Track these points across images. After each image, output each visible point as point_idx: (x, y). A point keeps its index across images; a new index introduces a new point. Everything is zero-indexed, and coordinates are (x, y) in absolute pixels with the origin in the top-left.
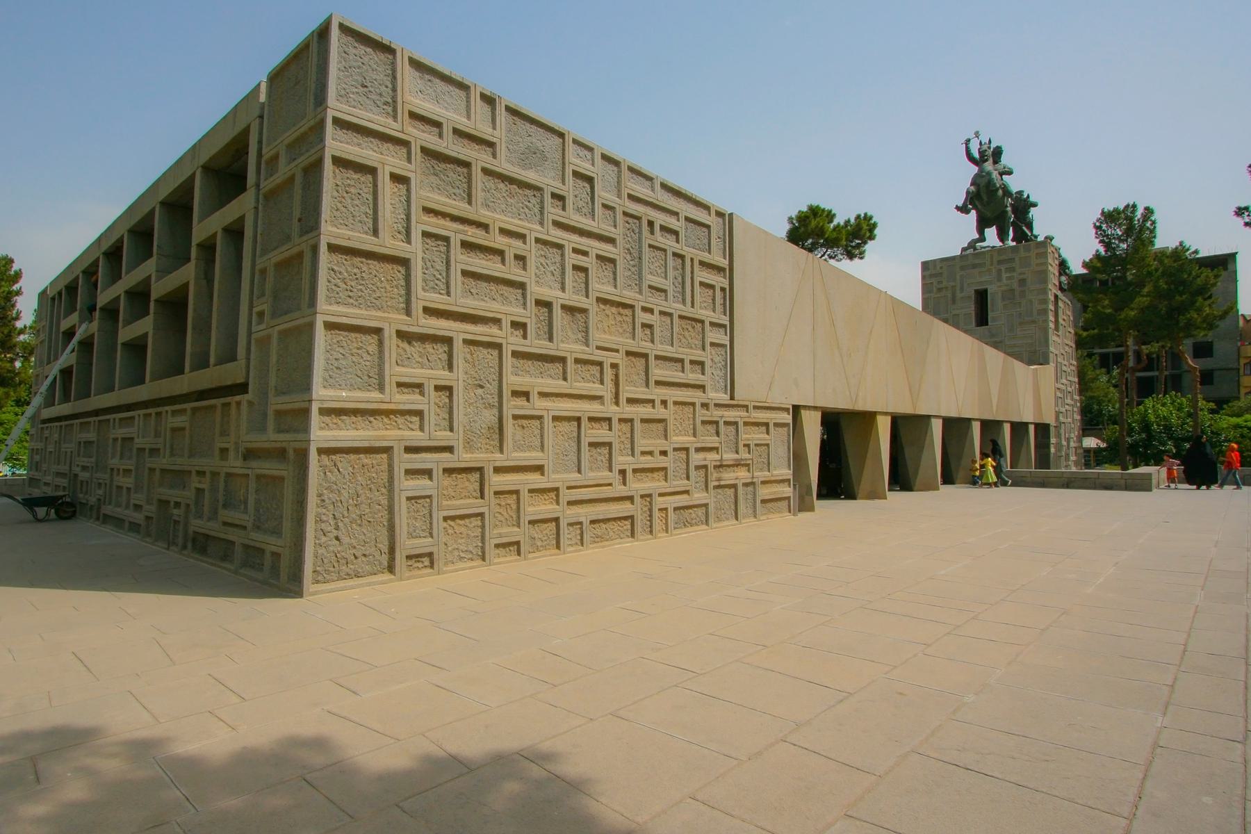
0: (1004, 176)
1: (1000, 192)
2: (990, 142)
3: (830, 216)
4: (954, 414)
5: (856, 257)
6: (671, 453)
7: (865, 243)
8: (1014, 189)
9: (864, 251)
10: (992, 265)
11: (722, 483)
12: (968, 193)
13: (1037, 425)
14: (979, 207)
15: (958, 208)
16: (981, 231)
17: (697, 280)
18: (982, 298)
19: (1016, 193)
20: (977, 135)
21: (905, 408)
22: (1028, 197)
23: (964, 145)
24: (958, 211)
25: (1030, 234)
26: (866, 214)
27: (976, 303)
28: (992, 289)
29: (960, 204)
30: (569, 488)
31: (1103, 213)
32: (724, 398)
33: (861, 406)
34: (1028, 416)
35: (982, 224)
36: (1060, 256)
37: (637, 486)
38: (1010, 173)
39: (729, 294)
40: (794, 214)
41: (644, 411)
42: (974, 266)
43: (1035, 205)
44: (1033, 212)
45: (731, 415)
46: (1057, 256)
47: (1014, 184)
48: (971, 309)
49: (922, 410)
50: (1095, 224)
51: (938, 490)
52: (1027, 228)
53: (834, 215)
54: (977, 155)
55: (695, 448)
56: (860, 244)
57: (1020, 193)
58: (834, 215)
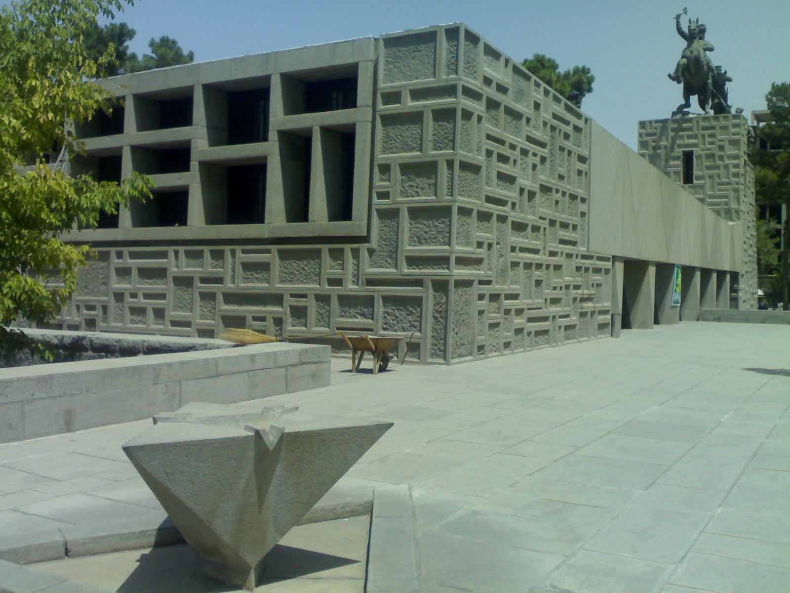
0: (707, 52)
1: (705, 67)
2: (697, 21)
3: (554, 66)
4: (687, 263)
8: (714, 63)
12: (679, 65)
14: (688, 77)
16: (687, 97)
18: (688, 158)
20: (685, 11)
22: (726, 73)
23: (676, 19)
24: (670, 78)
25: (725, 105)
31: (773, 87)
34: (727, 268)
35: (688, 93)
38: (711, 50)
43: (730, 80)
44: (728, 85)
47: (715, 59)
48: (678, 165)
49: (672, 261)
50: (767, 96)
51: (652, 328)
52: (724, 100)
54: (686, 30)
55: (574, 286)
56: (579, 95)
57: (718, 68)
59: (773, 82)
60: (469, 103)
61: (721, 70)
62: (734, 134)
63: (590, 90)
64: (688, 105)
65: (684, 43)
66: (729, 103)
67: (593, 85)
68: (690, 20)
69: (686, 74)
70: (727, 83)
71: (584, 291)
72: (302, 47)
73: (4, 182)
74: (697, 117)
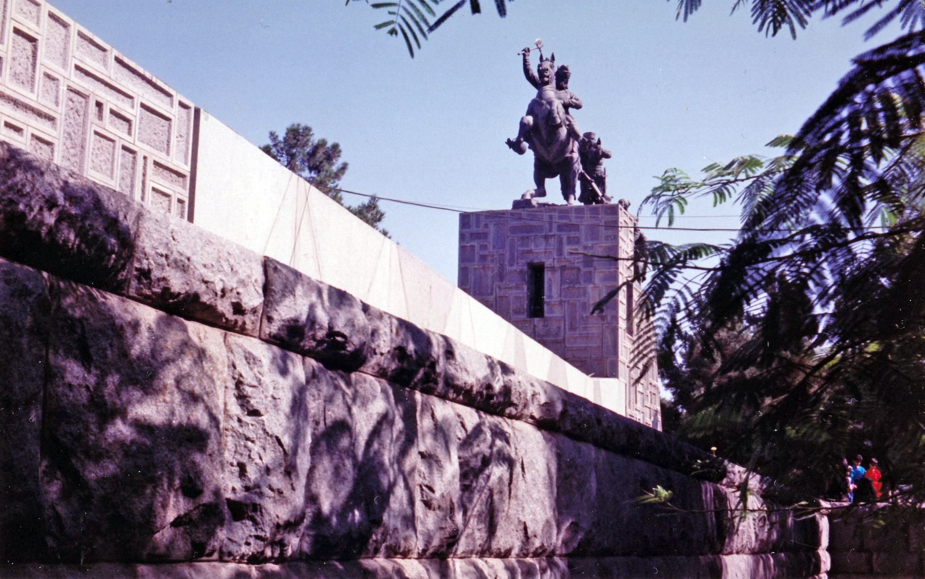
15: (510, 143)
16: (539, 180)
17: (150, 185)
22: (599, 142)
35: (542, 172)
54: (536, 74)
57: (588, 135)
65: (533, 92)
66: (608, 193)
70: (604, 161)
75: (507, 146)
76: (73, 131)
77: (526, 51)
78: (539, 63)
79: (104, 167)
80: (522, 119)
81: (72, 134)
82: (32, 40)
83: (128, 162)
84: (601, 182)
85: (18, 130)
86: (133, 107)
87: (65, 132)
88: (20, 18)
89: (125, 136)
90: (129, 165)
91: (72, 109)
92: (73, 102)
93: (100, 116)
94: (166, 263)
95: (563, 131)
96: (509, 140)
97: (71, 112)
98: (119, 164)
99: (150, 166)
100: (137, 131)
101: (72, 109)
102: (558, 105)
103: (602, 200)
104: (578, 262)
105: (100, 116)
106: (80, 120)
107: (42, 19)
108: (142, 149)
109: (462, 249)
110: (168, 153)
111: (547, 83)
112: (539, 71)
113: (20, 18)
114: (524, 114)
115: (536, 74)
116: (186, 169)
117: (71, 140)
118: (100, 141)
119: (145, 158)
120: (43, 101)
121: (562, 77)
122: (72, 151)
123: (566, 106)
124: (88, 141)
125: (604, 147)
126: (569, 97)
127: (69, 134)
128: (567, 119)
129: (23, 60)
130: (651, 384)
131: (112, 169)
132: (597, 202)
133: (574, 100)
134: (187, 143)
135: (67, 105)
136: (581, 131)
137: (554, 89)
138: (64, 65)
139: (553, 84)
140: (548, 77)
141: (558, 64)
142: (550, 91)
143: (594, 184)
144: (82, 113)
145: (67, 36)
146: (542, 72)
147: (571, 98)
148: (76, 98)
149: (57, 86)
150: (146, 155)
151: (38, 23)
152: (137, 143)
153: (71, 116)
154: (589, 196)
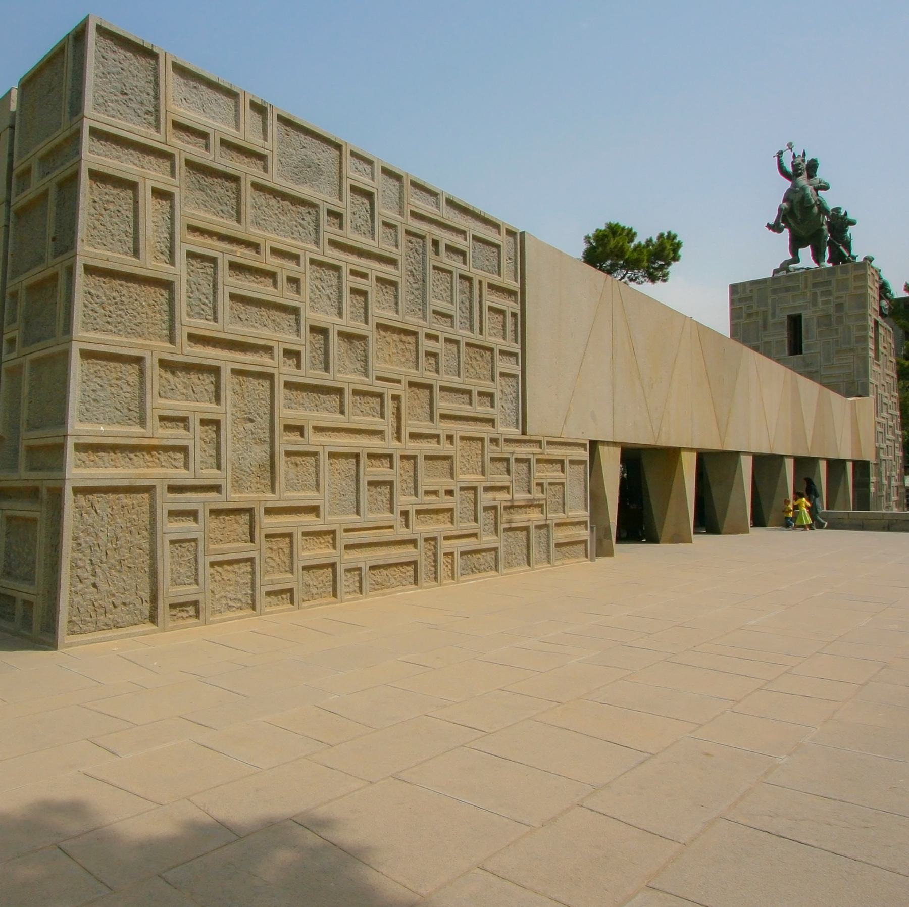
2: (804, 154)
3: (630, 235)
4: (765, 450)
5: (658, 279)
6: (457, 493)
7: (669, 264)
9: (668, 273)
10: (806, 287)
11: (513, 525)
13: (856, 463)
14: (793, 225)
15: (769, 226)
16: (794, 250)
17: (486, 304)
18: (795, 323)
19: (833, 210)
20: (790, 146)
21: (711, 444)
22: (846, 214)
23: (776, 158)
26: (669, 233)
27: (789, 329)
28: (808, 316)
29: (772, 222)
30: (346, 531)
32: (515, 433)
33: (663, 442)
34: (845, 452)
35: (796, 244)
36: (880, 278)
37: (421, 528)
38: (826, 188)
39: (520, 319)
40: (591, 232)
41: (429, 447)
42: (787, 290)
43: (853, 223)
45: (523, 451)
46: (877, 278)
53: (635, 234)
54: (790, 169)
57: (837, 210)
58: (635, 234)
59: (792, 142)
60: (130, 166)
61: (840, 212)
62: (856, 288)
63: (676, 258)
64: (796, 259)
65: (788, 184)
66: (853, 253)
67: (681, 252)
68: (794, 155)
69: (790, 221)
70: (850, 228)
71: (549, 515)
72: (862, 442)
73: (357, 576)
74: (805, 272)
75: (767, 229)
76: (415, 269)
77: (780, 154)
78: (792, 160)
79: (445, 295)
80: (780, 205)
81: (414, 271)
82: (369, 196)
83: (466, 288)
84: (848, 246)
85: (364, 276)
86: (465, 240)
87: (407, 270)
88: (356, 175)
89: (461, 265)
90: (467, 290)
91: (411, 250)
92: (412, 243)
93: (437, 253)
94: (390, 201)
95: (815, 209)
96: (768, 224)
97: (411, 253)
98: (458, 291)
99: (485, 286)
100: (471, 259)
101: (411, 250)
102: (810, 190)
103: (848, 259)
104: (832, 310)
105: (437, 253)
106: (420, 258)
107: (376, 174)
108: (477, 274)
109: (732, 310)
110: (499, 275)
111: (800, 174)
112: (793, 165)
113: (356, 175)
114: (781, 202)
115: (790, 169)
116: (515, 286)
117: (413, 276)
118: (439, 273)
119: (480, 282)
120: (384, 246)
121: (812, 167)
122: (415, 286)
123: (816, 189)
124: (428, 275)
125: (850, 216)
126: (818, 182)
127: (411, 271)
128: (819, 200)
129: (363, 212)
130: (893, 396)
131: (452, 296)
132: (844, 262)
133: (822, 184)
134: (516, 263)
135: (407, 247)
136: (830, 206)
137: (806, 179)
138: (401, 213)
139: (805, 175)
140: (801, 169)
141: (807, 158)
142: (803, 180)
143: (841, 248)
144: (421, 251)
145: (402, 187)
146: (795, 166)
147: (820, 183)
148: (413, 240)
149: (396, 231)
150: (481, 279)
151: (373, 179)
152: (473, 270)
153: (411, 256)
154: (837, 258)
